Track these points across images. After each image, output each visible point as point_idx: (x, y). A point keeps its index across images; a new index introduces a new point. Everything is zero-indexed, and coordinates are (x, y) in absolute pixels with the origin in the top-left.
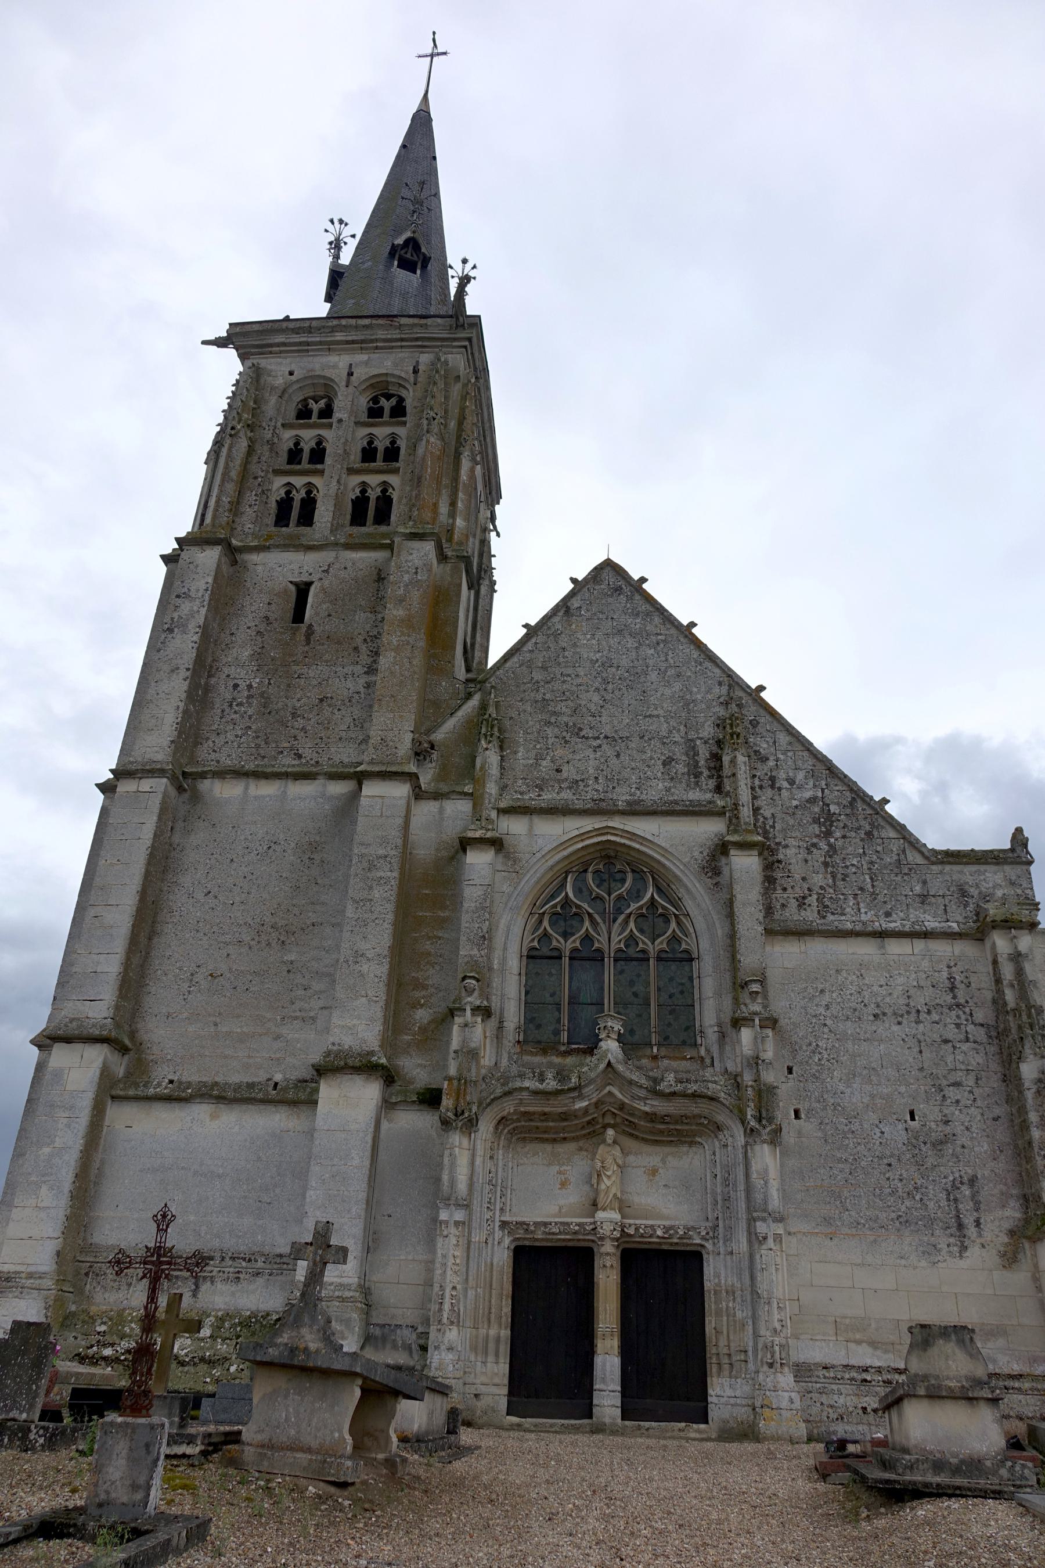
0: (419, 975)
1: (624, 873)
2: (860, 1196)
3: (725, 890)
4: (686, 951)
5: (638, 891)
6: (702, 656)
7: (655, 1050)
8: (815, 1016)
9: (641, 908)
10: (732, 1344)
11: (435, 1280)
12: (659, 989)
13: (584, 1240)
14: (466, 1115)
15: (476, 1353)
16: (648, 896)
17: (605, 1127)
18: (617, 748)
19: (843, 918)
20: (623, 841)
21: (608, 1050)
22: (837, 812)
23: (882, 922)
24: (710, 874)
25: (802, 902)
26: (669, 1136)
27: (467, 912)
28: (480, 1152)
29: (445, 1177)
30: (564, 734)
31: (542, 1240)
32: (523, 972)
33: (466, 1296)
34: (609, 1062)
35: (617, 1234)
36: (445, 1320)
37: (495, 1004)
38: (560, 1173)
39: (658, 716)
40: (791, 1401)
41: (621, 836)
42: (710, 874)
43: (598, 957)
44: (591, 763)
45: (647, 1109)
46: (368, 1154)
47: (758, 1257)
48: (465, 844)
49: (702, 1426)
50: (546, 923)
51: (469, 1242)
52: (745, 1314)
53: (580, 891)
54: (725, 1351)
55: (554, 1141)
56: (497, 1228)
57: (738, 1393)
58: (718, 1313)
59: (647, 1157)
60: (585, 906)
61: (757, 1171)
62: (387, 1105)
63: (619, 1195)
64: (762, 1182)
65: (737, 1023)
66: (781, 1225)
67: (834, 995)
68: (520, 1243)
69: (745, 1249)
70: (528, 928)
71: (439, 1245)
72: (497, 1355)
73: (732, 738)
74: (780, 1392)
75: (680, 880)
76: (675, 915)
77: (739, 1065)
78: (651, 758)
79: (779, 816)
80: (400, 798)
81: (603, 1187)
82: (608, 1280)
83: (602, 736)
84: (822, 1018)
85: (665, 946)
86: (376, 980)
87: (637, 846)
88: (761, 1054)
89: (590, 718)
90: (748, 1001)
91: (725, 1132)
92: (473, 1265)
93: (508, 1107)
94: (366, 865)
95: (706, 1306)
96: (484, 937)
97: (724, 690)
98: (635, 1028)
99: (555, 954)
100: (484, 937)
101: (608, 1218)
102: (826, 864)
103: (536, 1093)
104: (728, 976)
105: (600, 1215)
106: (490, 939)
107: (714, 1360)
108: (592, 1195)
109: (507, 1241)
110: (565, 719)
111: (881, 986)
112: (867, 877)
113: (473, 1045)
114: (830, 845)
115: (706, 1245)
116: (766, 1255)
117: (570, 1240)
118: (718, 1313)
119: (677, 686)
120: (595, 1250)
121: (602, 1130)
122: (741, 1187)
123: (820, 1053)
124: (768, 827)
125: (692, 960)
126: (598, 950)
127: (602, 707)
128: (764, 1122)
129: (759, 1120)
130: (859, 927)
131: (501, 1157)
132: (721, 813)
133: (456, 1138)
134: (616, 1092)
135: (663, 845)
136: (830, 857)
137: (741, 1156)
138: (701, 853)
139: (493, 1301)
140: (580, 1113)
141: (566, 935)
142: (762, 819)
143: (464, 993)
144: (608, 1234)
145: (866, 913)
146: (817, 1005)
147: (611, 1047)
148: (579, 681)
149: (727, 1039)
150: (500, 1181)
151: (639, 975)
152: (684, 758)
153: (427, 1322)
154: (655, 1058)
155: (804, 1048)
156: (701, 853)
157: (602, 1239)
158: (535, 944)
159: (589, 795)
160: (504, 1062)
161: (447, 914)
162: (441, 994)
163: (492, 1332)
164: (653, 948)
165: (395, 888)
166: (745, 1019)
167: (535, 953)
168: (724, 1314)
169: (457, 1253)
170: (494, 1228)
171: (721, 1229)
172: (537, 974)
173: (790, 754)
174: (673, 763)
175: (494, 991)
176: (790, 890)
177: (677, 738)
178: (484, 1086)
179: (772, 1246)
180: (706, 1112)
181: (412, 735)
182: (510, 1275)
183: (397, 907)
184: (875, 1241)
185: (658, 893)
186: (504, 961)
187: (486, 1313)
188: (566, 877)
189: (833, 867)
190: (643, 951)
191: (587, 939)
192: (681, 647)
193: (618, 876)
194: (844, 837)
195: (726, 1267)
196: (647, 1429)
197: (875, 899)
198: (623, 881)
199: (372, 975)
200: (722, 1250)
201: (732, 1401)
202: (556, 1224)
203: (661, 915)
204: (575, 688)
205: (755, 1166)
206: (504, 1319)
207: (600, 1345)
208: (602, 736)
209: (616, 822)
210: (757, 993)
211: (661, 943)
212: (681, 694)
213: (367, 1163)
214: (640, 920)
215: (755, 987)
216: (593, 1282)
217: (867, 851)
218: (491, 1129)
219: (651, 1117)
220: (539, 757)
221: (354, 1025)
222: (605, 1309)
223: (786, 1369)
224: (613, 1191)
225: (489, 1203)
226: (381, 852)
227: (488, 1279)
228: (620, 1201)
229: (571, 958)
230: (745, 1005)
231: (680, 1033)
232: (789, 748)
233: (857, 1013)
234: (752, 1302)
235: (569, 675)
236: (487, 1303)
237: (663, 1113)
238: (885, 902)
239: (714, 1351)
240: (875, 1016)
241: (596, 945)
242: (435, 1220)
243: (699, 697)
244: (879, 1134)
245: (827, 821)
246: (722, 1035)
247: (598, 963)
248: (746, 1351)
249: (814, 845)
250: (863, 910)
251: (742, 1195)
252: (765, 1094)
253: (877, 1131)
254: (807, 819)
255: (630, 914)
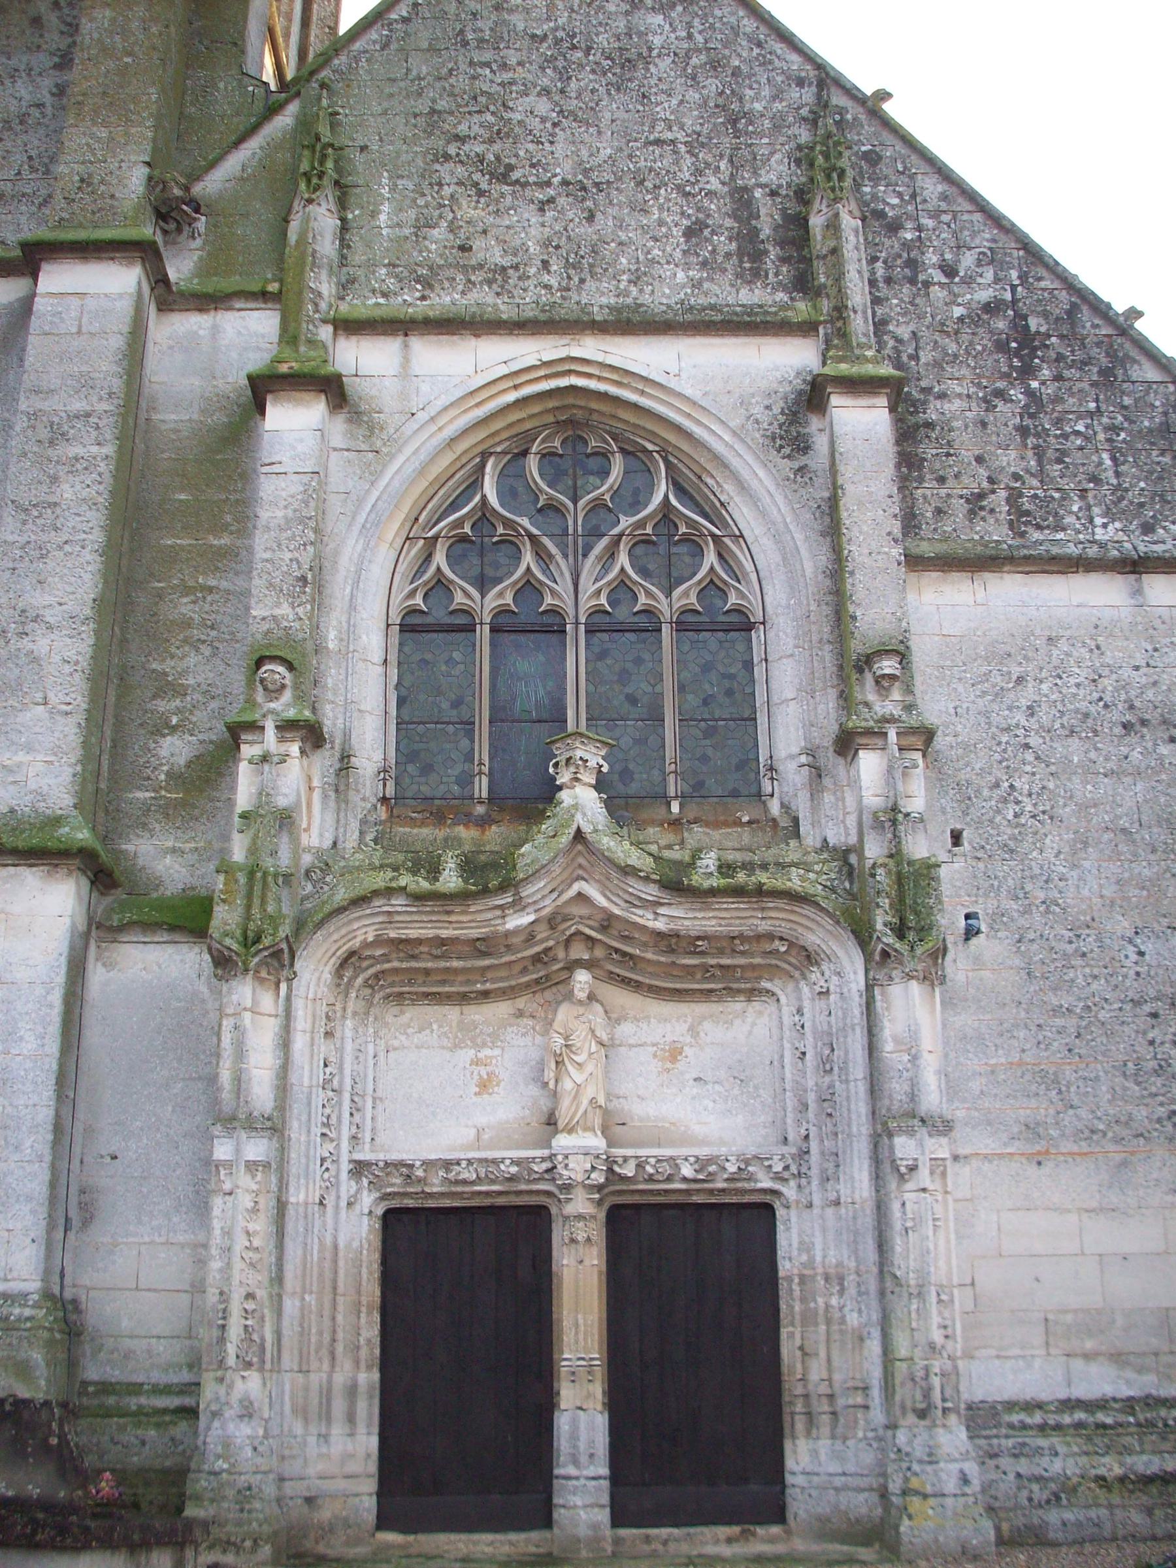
0: (168, 665)
1: (605, 455)
2: (1097, 1078)
3: (818, 482)
4: (738, 611)
5: (636, 492)
6: (762, 29)
7: (675, 807)
8: (1008, 729)
9: (641, 524)
10: (837, 1377)
11: (210, 1280)
12: (682, 688)
13: (531, 1192)
14: (266, 941)
15: (306, 1421)
16: (657, 499)
17: (571, 966)
18: (590, 204)
19: (1060, 536)
20: (602, 387)
21: (576, 806)
22: (1043, 329)
23: (1137, 542)
24: (787, 450)
25: (976, 503)
26: (705, 979)
27: (267, 528)
28: (302, 1021)
29: (225, 1076)
30: (477, 177)
31: (442, 1195)
32: (393, 658)
33: (279, 1312)
34: (579, 831)
35: (599, 1178)
36: (231, 1361)
37: (331, 720)
38: (476, 1062)
39: (673, 142)
40: (965, 1480)
41: (599, 378)
42: (787, 450)
43: (552, 627)
44: (533, 232)
45: (660, 925)
46: (55, 1028)
47: (896, 1206)
48: (263, 388)
49: (775, 1530)
50: (440, 558)
51: (281, 1206)
52: (864, 1320)
53: (514, 493)
54: (823, 1389)
55: (463, 999)
56: (344, 1175)
57: (851, 1468)
58: (809, 1318)
59: (655, 1024)
60: (525, 522)
61: (896, 1040)
62: (100, 930)
63: (601, 1101)
64: (906, 1058)
65: (847, 744)
66: (944, 1140)
67: (1044, 687)
68: (395, 1203)
69: (866, 1194)
70: (401, 568)
71: (216, 1212)
72: (351, 1418)
73: (829, 178)
74: (942, 1465)
75: (724, 465)
76: (713, 535)
77: (854, 832)
78: (661, 223)
79: (924, 333)
80: (121, 296)
81: (567, 1085)
82: (579, 1270)
83: (556, 180)
84: (1021, 732)
85: (693, 599)
86: (67, 669)
87: (633, 397)
88: (901, 802)
89: (531, 147)
90: (871, 697)
91: (825, 966)
92: (293, 1251)
93: (362, 929)
94: (44, 434)
95: (783, 1306)
96: (303, 579)
97: (808, 95)
98: (631, 766)
99: (461, 620)
100: (303, 579)
101: (579, 1149)
102: (1023, 431)
103: (419, 898)
104: (827, 654)
105: (562, 1142)
106: (320, 588)
107: (799, 1408)
108: (545, 1104)
109: (367, 1200)
110: (479, 149)
111: (1137, 668)
112: (1105, 456)
113: (282, 802)
114: (1029, 393)
115: (784, 1190)
116: (907, 1201)
117: (500, 1193)
118: (809, 1318)
119: (712, 85)
120: (554, 1210)
121: (564, 975)
122: (858, 1070)
123: (1017, 802)
124: (905, 358)
125: (748, 627)
126: (553, 611)
127: (555, 125)
128: (911, 936)
129: (900, 931)
130: (1093, 552)
131: (349, 1034)
132: (807, 328)
133: (243, 991)
134: (593, 892)
135: (688, 392)
136: (1032, 416)
137: (857, 1012)
138: (768, 407)
139: (340, 1318)
140: (516, 940)
141: (483, 584)
142: (891, 343)
143: (260, 696)
144: (580, 1177)
145: (1105, 526)
146: (1010, 708)
147: (582, 802)
148: (507, 76)
149: (827, 781)
150: (348, 1082)
151: (638, 661)
152: (729, 222)
153: (194, 1364)
154: (676, 824)
155: (986, 792)
156: (768, 407)
157: (567, 1188)
158: (418, 600)
159: (528, 298)
160: (351, 841)
161: (225, 540)
162: (214, 705)
163: (340, 1379)
164: (667, 606)
165: (108, 479)
166: (869, 732)
167: (416, 620)
168: (821, 1319)
169: (252, 1227)
170: (337, 1176)
171: (815, 1157)
172: (424, 661)
173: (945, 218)
174: (706, 232)
175: (330, 696)
176: (951, 482)
177: (714, 184)
178: (309, 888)
179: (927, 1183)
180: (784, 928)
181: (146, 170)
182: (376, 1266)
183: (110, 517)
184: (1124, 1164)
185: (676, 496)
186: (350, 633)
187: (327, 1337)
188: (481, 467)
189: (1037, 435)
190: (647, 612)
191: (529, 588)
192: (718, 13)
193: (593, 463)
194: (1058, 378)
195: (824, 1230)
196: (665, 1543)
197: (1122, 498)
198: (605, 473)
199: (56, 658)
200: (817, 1199)
201: (839, 1481)
202: (470, 1162)
203: (686, 539)
204: (495, 88)
205: (889, 1030)
206: (364, 1353)
207: (568, 1395)
208: (556, 180)
209: (589, 347)
210: (892, 677)
211: (686, 594)
212: (720, 101)
213: (53, 1047)
214: (640, 550)
215: (888, 666)
216: (549, 1273)
217: (1103, 407)
218: (327, 976)
219: (668, 941)
220: (423, 225)
221: (19, 765)
222: (577, 1325)
223: (953, 1419)
224: (589, 1092)
225: (327, 1125)
226: (78, 405)
227: (328, 1274)
228: (606, 1113)
229: (493, 630)
230: (867, 704)
231: (728, 773)
232: (943, 206)
233: (1090, 722)
234: (882, 1293)
235: (487, 65)
236: (327, 1322)
237: (693, 933)
238: (1142, 505)
239: (799, 1390)
240: (1126, 726)
241: (549, 600)
242: (210, 1165)
243: (758, 106)
244: (1134, 957)
245: (1023, 348)
246: (817, 773)
247: (554, 638)
248: (865, 1389)
249: (1000, 394)
250: (1099, 521)
251: (860, 1089)
252: (913, 884)
253: (1131, 950)
254: (984, 341)
255: (621, 535)
